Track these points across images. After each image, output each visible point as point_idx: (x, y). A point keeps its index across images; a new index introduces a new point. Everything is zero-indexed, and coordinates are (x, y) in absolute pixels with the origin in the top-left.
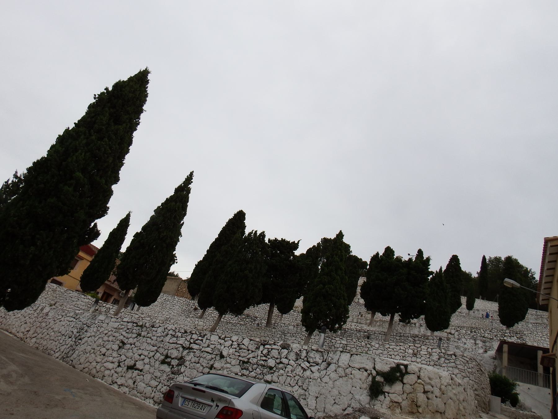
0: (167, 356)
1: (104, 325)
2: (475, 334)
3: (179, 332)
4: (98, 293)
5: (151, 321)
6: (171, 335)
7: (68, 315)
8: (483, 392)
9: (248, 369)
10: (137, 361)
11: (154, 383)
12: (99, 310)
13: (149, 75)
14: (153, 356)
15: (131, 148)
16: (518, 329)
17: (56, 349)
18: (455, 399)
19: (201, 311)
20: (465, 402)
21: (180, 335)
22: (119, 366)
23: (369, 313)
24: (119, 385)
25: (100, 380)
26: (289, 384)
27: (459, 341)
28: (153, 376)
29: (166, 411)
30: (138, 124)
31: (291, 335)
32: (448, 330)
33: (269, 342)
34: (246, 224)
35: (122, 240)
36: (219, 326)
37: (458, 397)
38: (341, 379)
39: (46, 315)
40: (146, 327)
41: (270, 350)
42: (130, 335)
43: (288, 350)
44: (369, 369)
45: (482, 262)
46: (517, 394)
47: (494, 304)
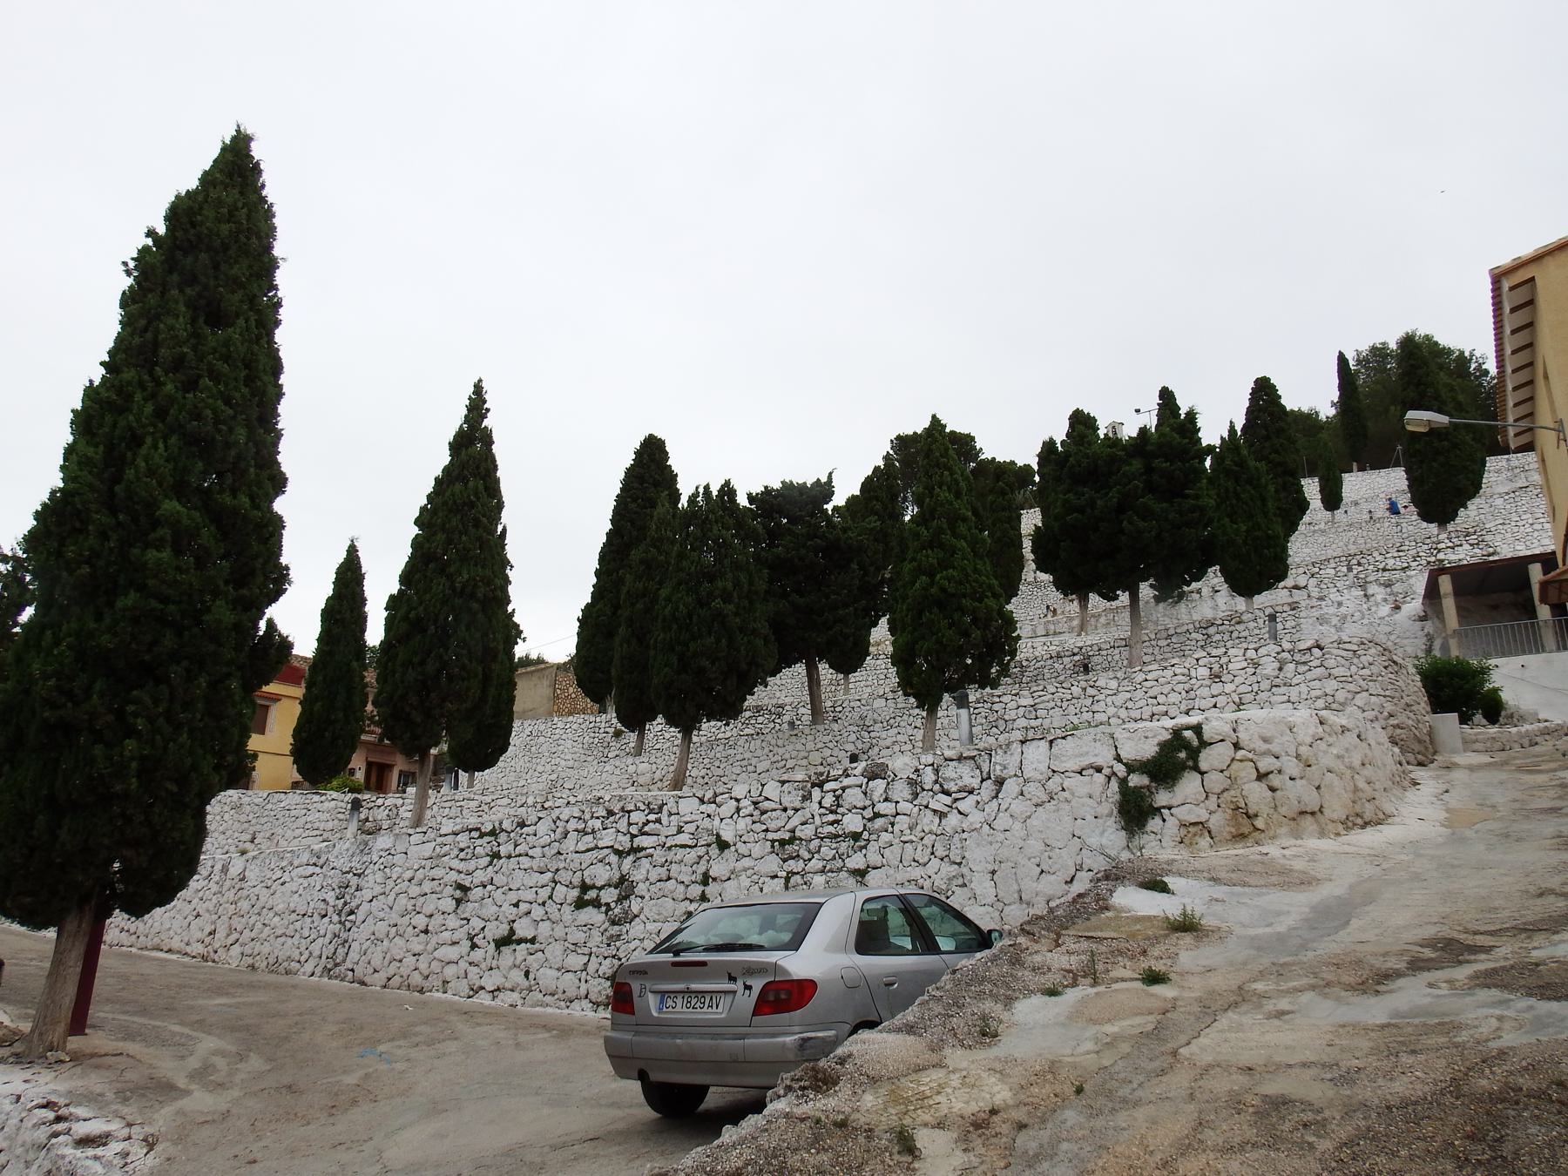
0: (585, 888)
1: (399, 859)
2: (1361, 568)
3: (592, 817)
4: (352, 772)
5: (513, 804)
6: (576, 830)
7: (296, 863)
8: (1411, 715)
9: (798, 856)
10: (514, 921)
11: (576, 961)
12: (370, 819)
13: (253, 145)
14: (550, 897)
15: (283, 380)
16: (1470, 519)
17: (301, 954)
18: (1342, 767)
19: (632, 737)
20: (1368, 766)
21: (598, 824)
22: (474, 946)
23: (1072, 601)
24: (492, 992)
25: (439, 995)
26: (914, 861)
27: (1324, 603)
28: (566, 944)
29: (628, 1036)
30: (279, 305)
31: (885, 724)
32: (1289, 582)
33: (832, 774)
34: (675, 469)
35: (361, 621)
36: (692, 761)
37: (1346, 760)
38: (1040, 809)
39: (240, 880)
40: (507, 832)
41: (840, 792)
42: (472, 865)
43: (884, 778)
44: (1105, 765)
45: (1340, 371)
46: (1496, 690)
47: (1393, 475)
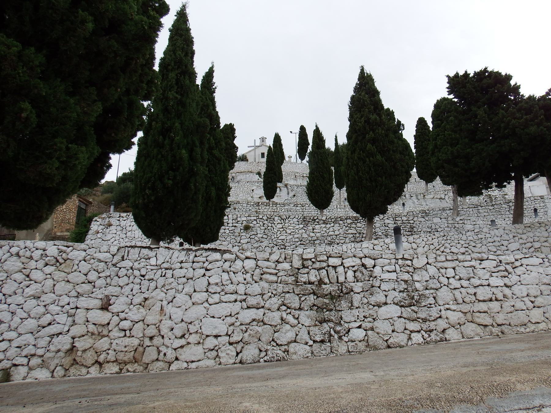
34: (379, 89)
